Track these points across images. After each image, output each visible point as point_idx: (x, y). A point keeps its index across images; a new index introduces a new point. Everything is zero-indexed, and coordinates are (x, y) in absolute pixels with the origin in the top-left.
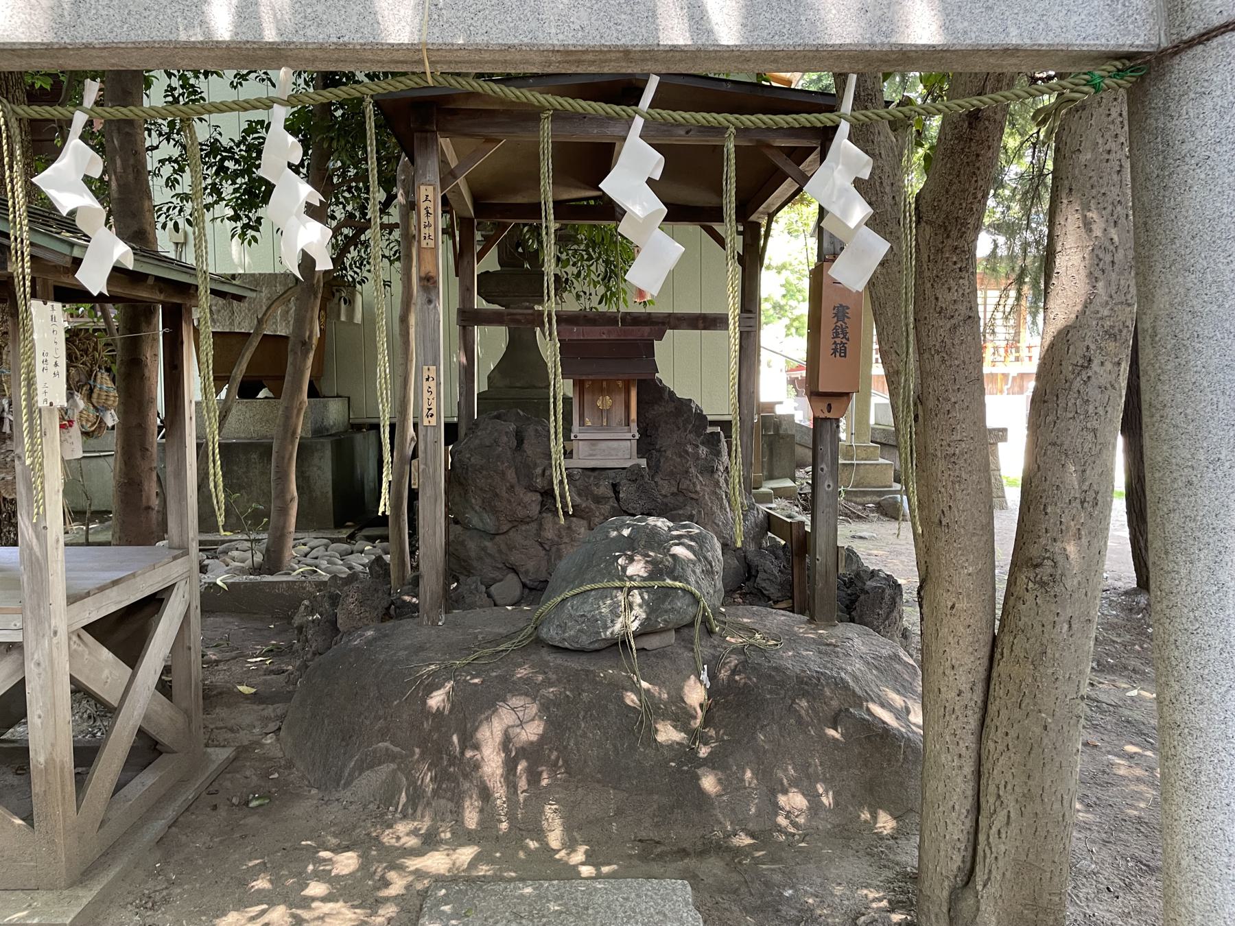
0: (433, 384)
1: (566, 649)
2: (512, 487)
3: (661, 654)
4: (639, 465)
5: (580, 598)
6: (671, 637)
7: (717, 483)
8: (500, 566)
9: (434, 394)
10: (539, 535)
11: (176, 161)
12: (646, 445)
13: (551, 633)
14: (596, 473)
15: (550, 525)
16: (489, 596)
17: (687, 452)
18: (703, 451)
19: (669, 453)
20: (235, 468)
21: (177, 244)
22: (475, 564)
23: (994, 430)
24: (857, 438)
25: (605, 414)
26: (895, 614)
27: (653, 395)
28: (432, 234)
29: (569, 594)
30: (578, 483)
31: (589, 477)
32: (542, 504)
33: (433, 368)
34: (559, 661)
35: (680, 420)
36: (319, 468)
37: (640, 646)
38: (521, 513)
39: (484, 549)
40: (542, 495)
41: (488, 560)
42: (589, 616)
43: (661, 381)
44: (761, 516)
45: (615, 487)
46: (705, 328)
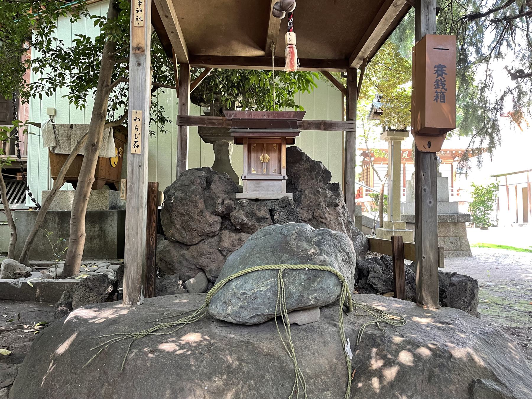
0: (139, 123)
1: (230, 324)
2: (202, 211)
3: (309, 328)
4: (287, 197)
5: (242, 280)
6: (316, 314)
7: (338, 214)
8: (193, 267)
9: (140, 131)
10: (219, 245)
11: (41, 61)
12: (291, 186)
13: (216, 310)
14: (259, 203)
15: (227, 238)
16: (185, 287)
17: (318, 192)
18: (329, 193)
19: (307, 192)
20: (66, 225)
21: (51, 116)
22: (177, 266)
23: (463, 215)
24: (394, 218)
25: (265, 166)
26: (475, 301)
27: (295, 157)
28: (142, 16)
29: (234, 276)
30: (246, 209)
31: (254, 205)
32: (222, 224)
33: (139, 112)
34: (224, 334)
35: (314, 174)
36: (111, 225)
37: (293, 322)
38: (207, 229)
39: (183, 255)
40: (222, 218)
41: (185, 263)
42: (250, 293)
43: (301, 150)
44: (364, 239)
45: (271, 212)
46: (325, 129)
